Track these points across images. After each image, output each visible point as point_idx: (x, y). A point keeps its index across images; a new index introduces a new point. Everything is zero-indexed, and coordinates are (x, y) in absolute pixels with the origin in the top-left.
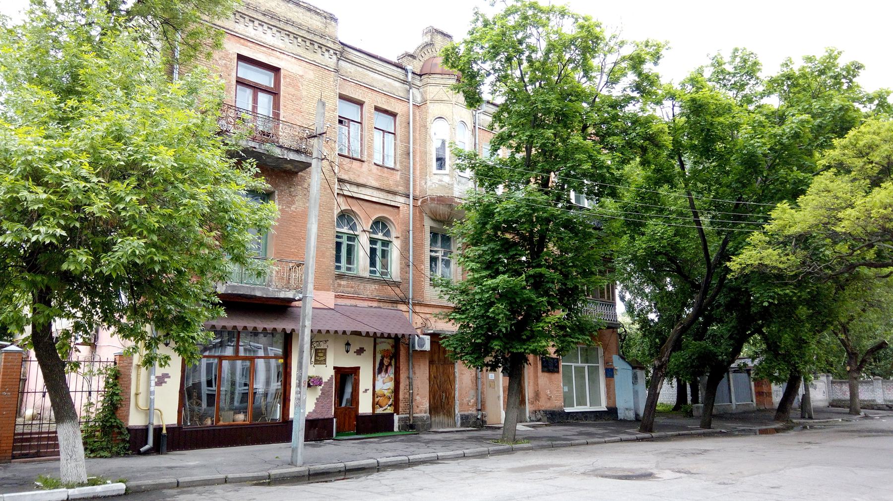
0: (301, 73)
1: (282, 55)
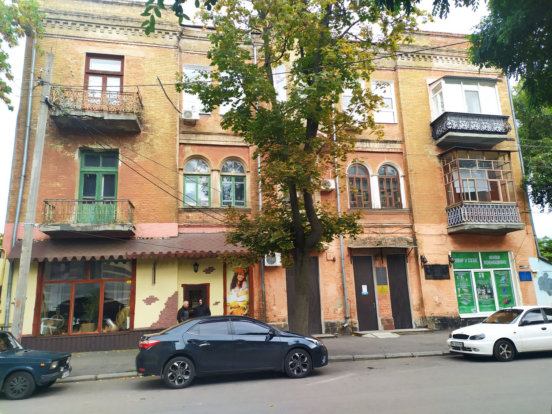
0: (142, 56)
1: (126, 46)
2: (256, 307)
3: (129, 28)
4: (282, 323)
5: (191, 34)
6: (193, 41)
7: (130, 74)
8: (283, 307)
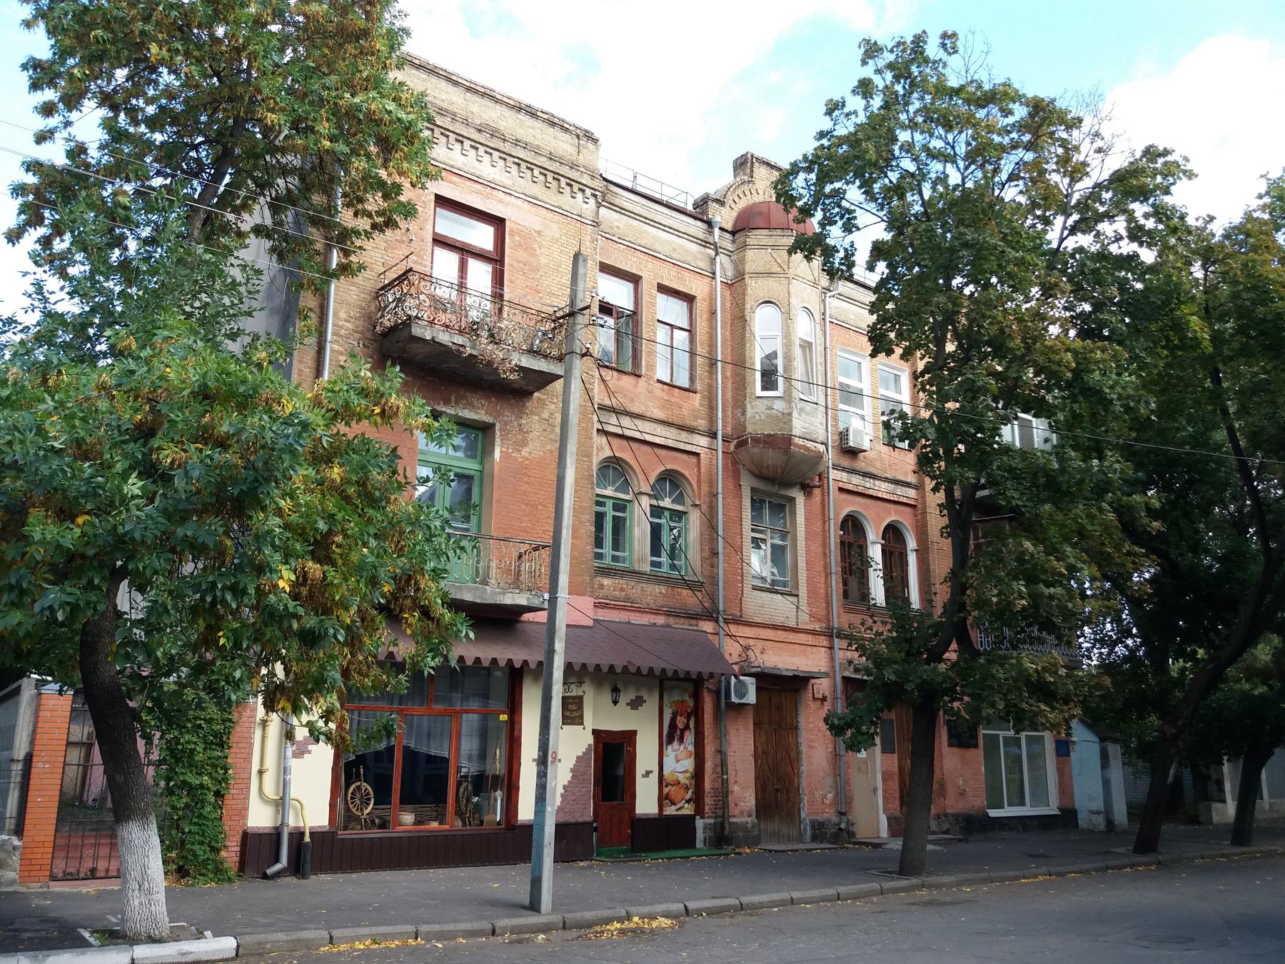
0: (538, 228)
1: (508, 197)
2: (708, 785)
3: (517, 160)
4: (749, 820)
5: (617, 201)
6: (617, 216)
7: (516, 264)
8: (749, 788)
